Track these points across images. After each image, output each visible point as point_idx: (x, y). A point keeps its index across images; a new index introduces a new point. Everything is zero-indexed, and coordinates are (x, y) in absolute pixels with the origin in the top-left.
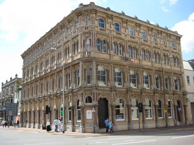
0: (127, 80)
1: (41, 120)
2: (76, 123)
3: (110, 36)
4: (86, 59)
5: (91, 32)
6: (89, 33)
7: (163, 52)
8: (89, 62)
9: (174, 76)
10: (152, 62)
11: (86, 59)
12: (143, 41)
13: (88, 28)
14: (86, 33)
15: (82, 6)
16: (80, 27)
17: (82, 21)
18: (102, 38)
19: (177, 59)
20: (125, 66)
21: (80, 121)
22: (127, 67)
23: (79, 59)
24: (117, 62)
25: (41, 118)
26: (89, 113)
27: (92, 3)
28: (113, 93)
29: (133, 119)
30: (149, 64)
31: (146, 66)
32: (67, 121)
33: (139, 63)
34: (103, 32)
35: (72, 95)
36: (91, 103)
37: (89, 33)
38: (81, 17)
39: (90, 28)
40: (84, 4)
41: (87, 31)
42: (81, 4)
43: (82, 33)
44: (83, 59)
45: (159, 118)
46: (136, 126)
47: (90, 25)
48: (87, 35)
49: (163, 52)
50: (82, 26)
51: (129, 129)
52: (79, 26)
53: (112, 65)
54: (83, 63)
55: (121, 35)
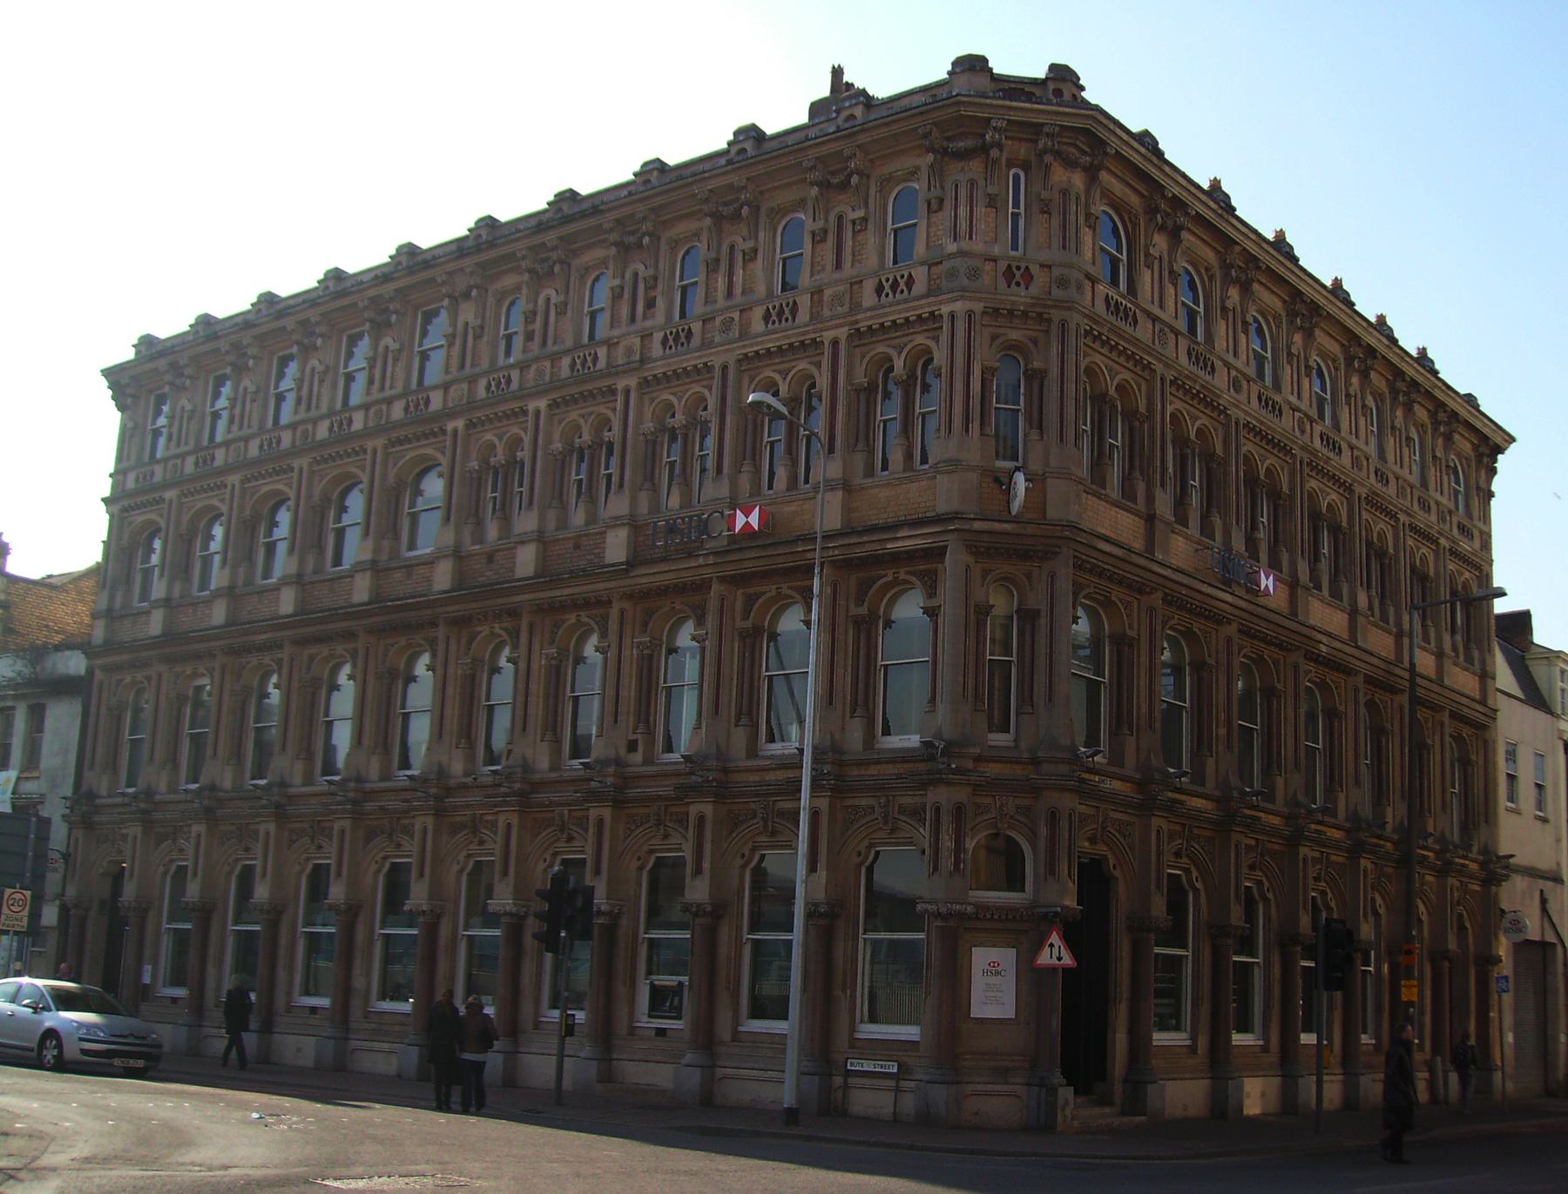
0: (1223, 731)
1: (289, 994)
2: (853, 1042)
3: (1159, 367)
4: (1006, 527)
5: (1056, 315)
6: (1040, 315)
7: (1169, 409)
8: (1025, 555)
9: (1077, 588)
10: (1150, 519)
11: (1006, 527)
12: (1100, 307)
13: (1028, 277)
14: (1011, 312)
15: (982, 82)
16: (962, 253)
17: (980, 210)
18: (1194, 419)
19: (1335, 530)
20: (1218, 619)
21: (181, 992)
22: (1232, 629)
23: (938, 520)
24: (1186, 580)
25: (368, 975)
26: (994, 969)
27: (1063, 78)
28: (1156, 822)
29: (977, 1012)
30: (1121, 525)
31: (1324, 639)
32: (537, 1014)
33: (1286, 611)
34: (1122, 325)
35: (832, 807)
36: (1011, 895)
37: (1037, 316)
38: (975, 167)
39: (1040, 279)
40: (999, 66)
41: (1020, 297)
42: (972, 65)
43: (978, 307)
44: (977, 525)
45: (257, 928)
46: (299, 1050)
47: (1044, 256)
48: (1014, 335)
49: (1169, 409)
50: (977, 246)
51: (707, 1100)
52: (952, 247)
53: (1157, 599)
54: (971, 560)
55: (1136, 322)
